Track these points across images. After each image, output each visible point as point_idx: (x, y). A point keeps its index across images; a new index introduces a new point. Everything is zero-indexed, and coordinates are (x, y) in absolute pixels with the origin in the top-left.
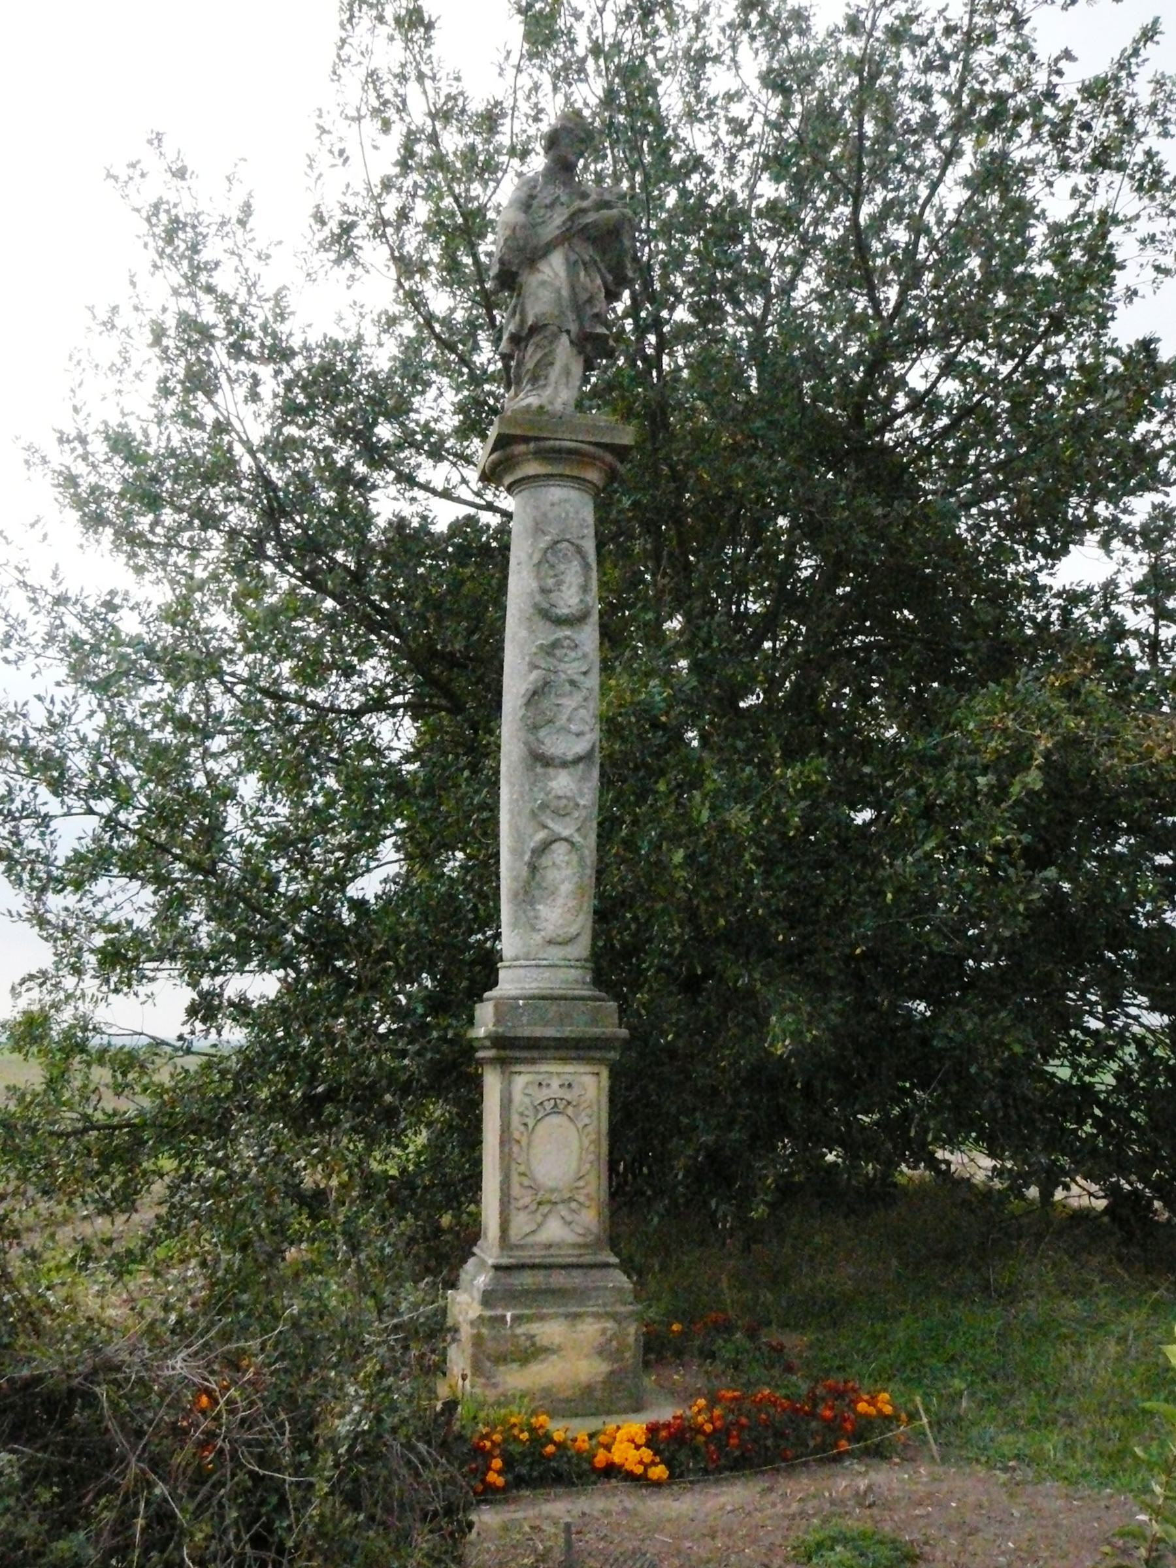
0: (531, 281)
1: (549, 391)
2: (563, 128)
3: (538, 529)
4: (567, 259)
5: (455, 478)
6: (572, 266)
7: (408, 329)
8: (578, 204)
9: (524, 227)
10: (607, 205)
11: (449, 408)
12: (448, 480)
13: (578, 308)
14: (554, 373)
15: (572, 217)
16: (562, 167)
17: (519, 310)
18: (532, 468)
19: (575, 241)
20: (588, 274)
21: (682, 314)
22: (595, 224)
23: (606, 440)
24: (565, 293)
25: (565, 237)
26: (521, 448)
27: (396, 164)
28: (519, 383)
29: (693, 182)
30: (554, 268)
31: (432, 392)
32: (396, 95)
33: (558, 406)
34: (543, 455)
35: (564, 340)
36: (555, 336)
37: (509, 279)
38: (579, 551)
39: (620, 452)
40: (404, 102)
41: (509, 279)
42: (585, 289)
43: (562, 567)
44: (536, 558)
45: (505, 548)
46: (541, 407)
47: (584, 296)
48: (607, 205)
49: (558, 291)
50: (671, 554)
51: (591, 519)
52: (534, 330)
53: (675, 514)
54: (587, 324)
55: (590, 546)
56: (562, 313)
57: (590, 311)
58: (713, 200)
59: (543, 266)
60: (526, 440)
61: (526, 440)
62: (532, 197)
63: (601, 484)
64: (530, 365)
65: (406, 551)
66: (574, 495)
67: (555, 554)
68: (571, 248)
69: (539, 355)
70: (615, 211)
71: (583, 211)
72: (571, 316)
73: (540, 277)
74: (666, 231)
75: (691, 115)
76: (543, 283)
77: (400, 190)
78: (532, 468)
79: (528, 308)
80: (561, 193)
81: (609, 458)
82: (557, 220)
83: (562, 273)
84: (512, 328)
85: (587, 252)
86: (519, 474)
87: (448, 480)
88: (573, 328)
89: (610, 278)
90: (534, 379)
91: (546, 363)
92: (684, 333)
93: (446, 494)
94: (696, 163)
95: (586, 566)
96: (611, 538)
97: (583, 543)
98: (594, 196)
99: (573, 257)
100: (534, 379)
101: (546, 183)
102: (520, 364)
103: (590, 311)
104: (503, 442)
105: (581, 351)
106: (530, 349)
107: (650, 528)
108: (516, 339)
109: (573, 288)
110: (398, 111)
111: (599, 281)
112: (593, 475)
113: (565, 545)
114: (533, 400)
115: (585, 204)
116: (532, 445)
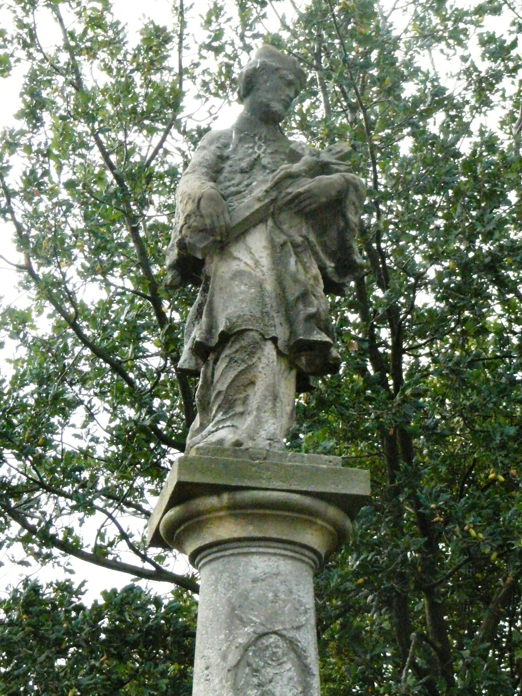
0: (221, 270)
1: (249, 420)
2: (264, 67)
3: (235, 616)
4: (271, 241)
5: (112, 532)
6: (278, 252)
7: (44, 326)
8: (286, 167)
9: (211, 198)
10: (324, 168)
11: (103, 435)
12: (101, 535)
13: (288, 309)
14: (256, 395)
15: (277, 185)
16: (265, 119)
17: (206, 310)
18: (226, 530)
19: (284, 216)
20: (299, 260)
21: (425, 299)
22: (309, 194)
23: (331, 489)
24: (269, 286)
25: (268, 213)
26: (213, 501)
27: (19, 116)
28: (206, 408)
29: (435, 124)
30: (254, 253)
31: (78, 415)
32: (21, 25)
33: (262, 443)
34: (239, 511)
35: (269, 349)
36: (254, 349)
37: (191, 270)
38: (293, 645)
39: (349, 504)
40: (33, 36)
41: (191, 270)
42: (296, 281)
43: (270, 672)
44: (233, 658)
45: (189, 633)
46: (238, 444)
47: (293, 292)
48: (324, 168)
49: (260, 286)
50: (421, 637)
51: (308, 600)
52: (226, 338)
53: (427, 575)
54: (300, 328)
55: (308, 639)
56: (265, 314)
57: (304, 311)
58: (465, 146)
59: (239, 251)
60: (216, 490)
61: (216, 490)
62: (222, 158)
63: (322, 551)
64: (222, 386)
65: (41, 640)
66: (285, 566)
67: (260, 652)
68: (278, 225)
69: (231, 375)
70: (335, 176)
71: (291, 176)
72: (278, 319)
73: (234, 266)
74: (403, 187)
75: (428, 37)
76: (238, 275)
77: (28, 148)
78: (226, 530)
79: (219, 302)
80: (262, 151)
81: (332, 512)
82: (260, 186)
83: (265, 261)
84: (196, 333)
85: (298, 230)
86: (207, 538)
87: (101, 535)
88: (281, 332)
89: (330, 265)
90: (228, 405)
91: (244, 382)
92: (432, 326)
93: (99, 557)
94: (439, 99)
95: (304, 670)
96: (336, 620)
97: (298, 635)
98: (307, 158)
99: (280, 239)
100: (228, 405)
101: (241, 140)
102: (208, 384)
103: (304, 311)
104: (182, 494)
105: (292, 365)
106: (221, 365)
107: (396, 603)
108: (201, 350)
109: (280, 281)
110: (25, 45)
111: (315, 270)
112: (313, 538)
113: (273, 638)
114: (226, 435)
115: (296, 167)
116: (226, 497)
